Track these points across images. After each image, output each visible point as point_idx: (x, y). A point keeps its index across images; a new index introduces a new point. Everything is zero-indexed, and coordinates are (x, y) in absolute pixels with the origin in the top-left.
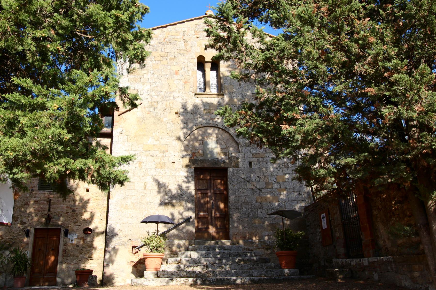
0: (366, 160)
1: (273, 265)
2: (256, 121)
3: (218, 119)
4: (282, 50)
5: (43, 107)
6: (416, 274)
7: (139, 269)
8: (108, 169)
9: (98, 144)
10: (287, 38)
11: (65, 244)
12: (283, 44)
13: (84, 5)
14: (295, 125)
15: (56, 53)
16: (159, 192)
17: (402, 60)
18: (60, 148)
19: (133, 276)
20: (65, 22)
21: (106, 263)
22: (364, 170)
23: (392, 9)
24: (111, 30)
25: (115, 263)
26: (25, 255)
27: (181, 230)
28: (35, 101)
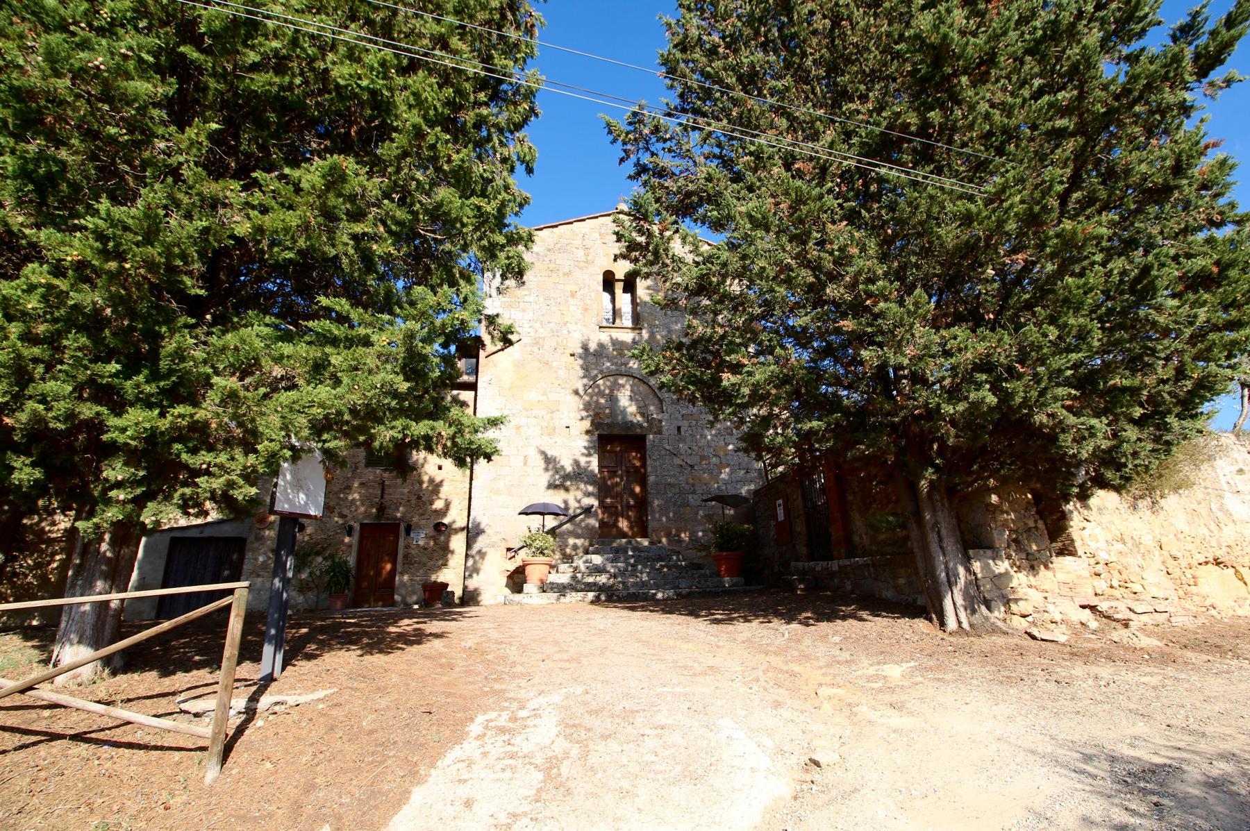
0: (838, 424)
1: (708, 572)
2: (687, 367)
3: (634, 364)
4: (724, 265)
5: (366, 342)
6: (902, 581)
7: (517, 580)
8: (468, 436)
9: (456, 400)
10: (732, 247)
11: (407, 547)
12: (725, 255)
13: (431, 189)
14: (740, 374)
15: (387, 259)
16: (546, 469)
17: (892, 282)
18: (394, 403)
19: (508, 591)
20: (401, 214)
21: (471, 571)
22: (835, 438)
23: (880, 208)
24: (471, 228)
25: (481, 573)
26: (346, 562)
27: (578, 525)
28: (354, 333)
